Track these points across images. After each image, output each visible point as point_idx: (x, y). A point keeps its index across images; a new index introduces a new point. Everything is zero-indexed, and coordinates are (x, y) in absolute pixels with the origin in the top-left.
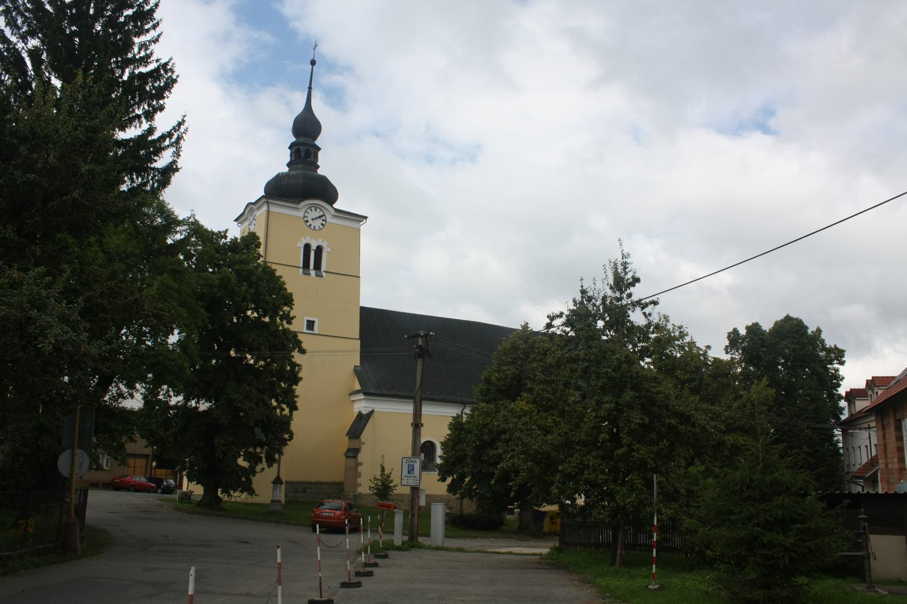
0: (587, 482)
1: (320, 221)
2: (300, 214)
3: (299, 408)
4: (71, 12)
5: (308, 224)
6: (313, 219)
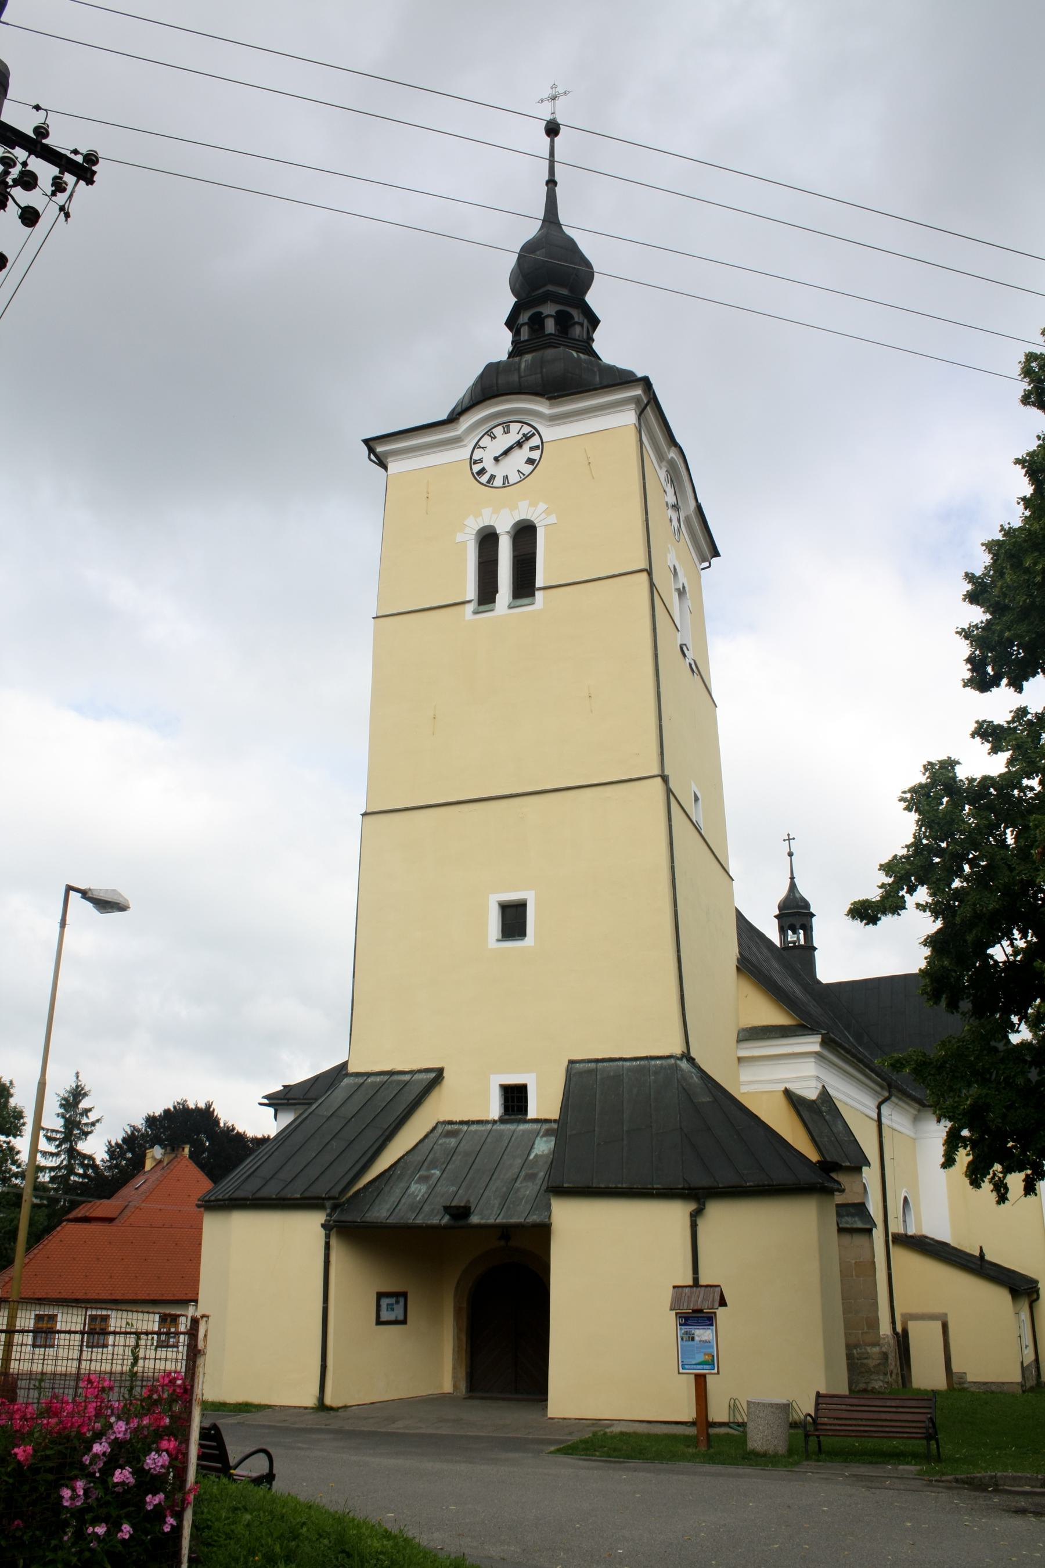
0: (150, 1381)
1: (520, 456)
2: (462, 453)
3: (721, 554)
4: (1019, 730)
5: (498, 482)
6: (496, 459)
